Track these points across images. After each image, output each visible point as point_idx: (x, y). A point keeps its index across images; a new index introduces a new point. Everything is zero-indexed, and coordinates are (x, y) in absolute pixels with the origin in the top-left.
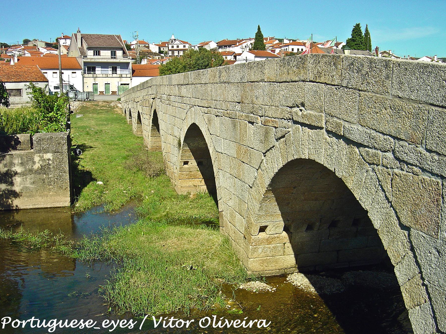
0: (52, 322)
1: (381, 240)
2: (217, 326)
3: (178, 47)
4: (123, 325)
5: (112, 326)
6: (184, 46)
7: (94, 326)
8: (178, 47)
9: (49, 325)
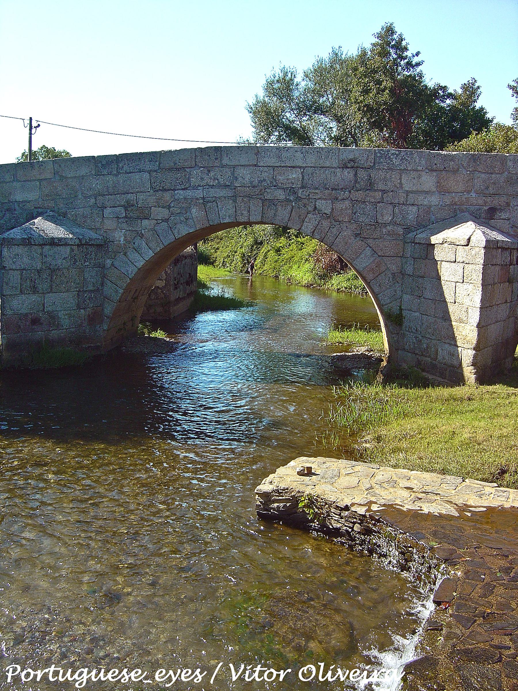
5: (170, 679)
9: (76, 676)
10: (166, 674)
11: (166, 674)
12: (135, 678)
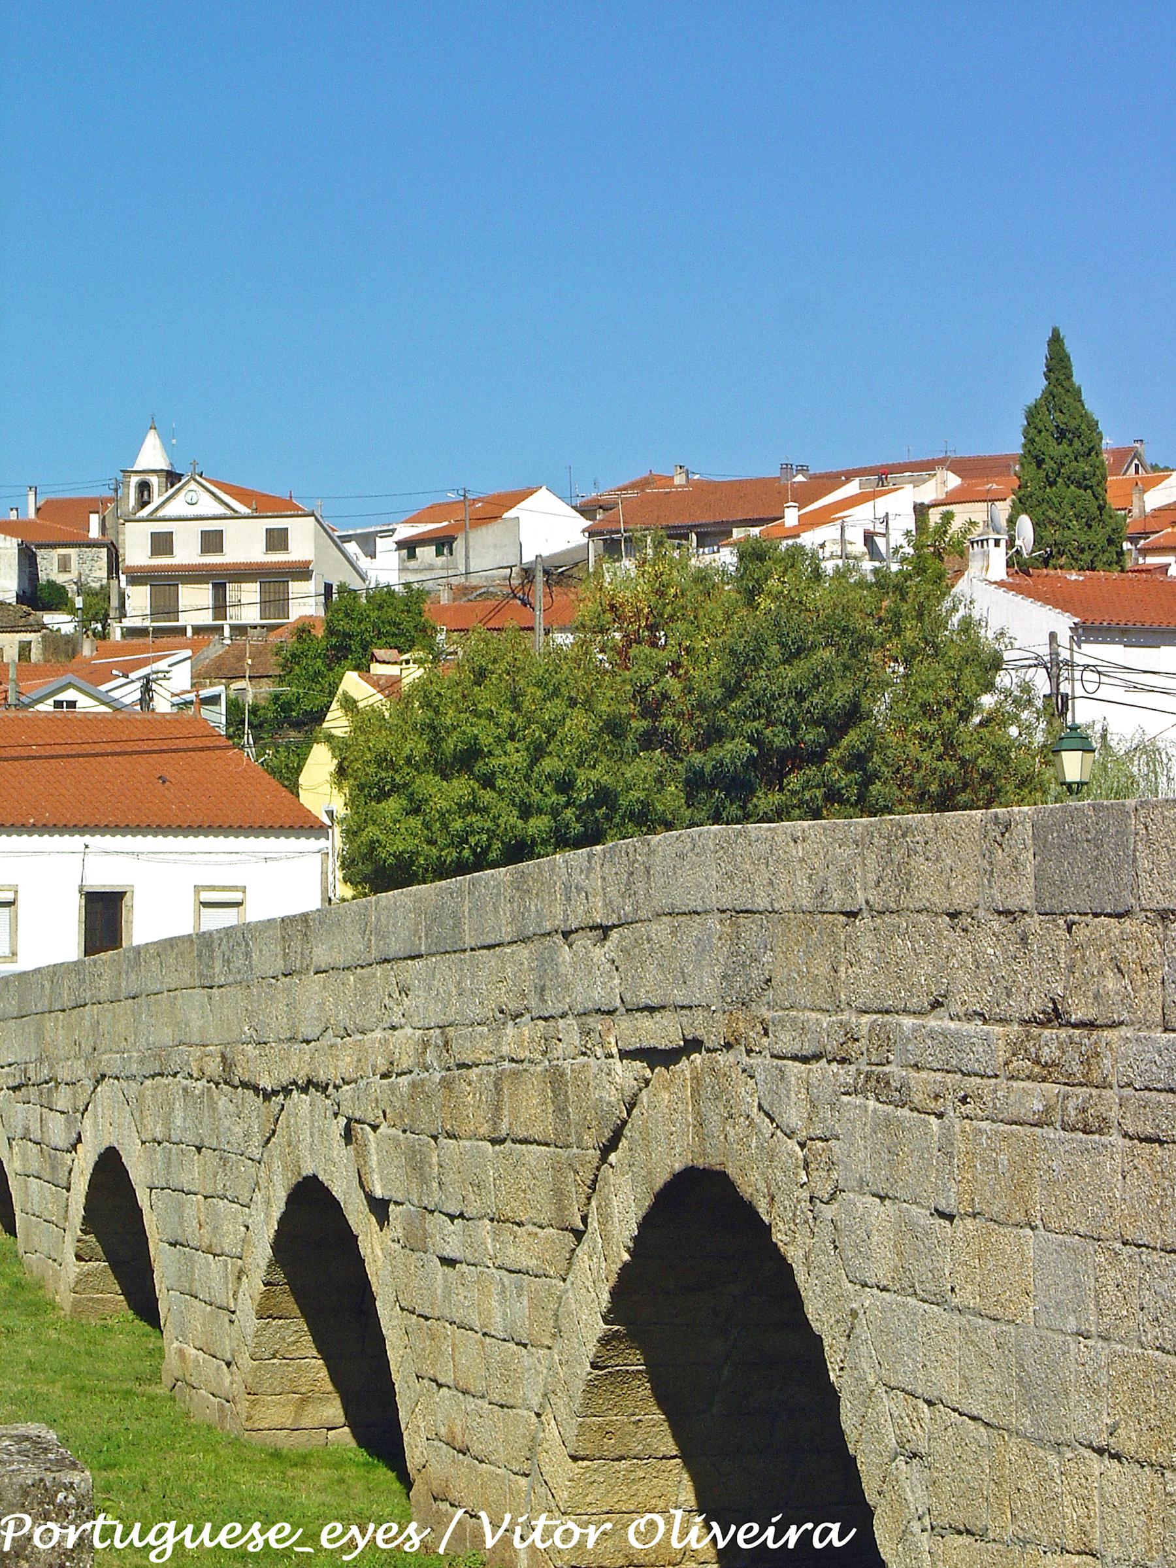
0: (161, 1533)
1: (382, 1339)
2: (198, 1542)
3: (212, 542)
4: (387, 1541)
5: (352, 1545)
6: (277, 540)
7: (296, 1544)
8: (212, 542)
9: (150, 1539)
10: (343, 1534)
11: (343, 1534)
12: (278, 1541)
